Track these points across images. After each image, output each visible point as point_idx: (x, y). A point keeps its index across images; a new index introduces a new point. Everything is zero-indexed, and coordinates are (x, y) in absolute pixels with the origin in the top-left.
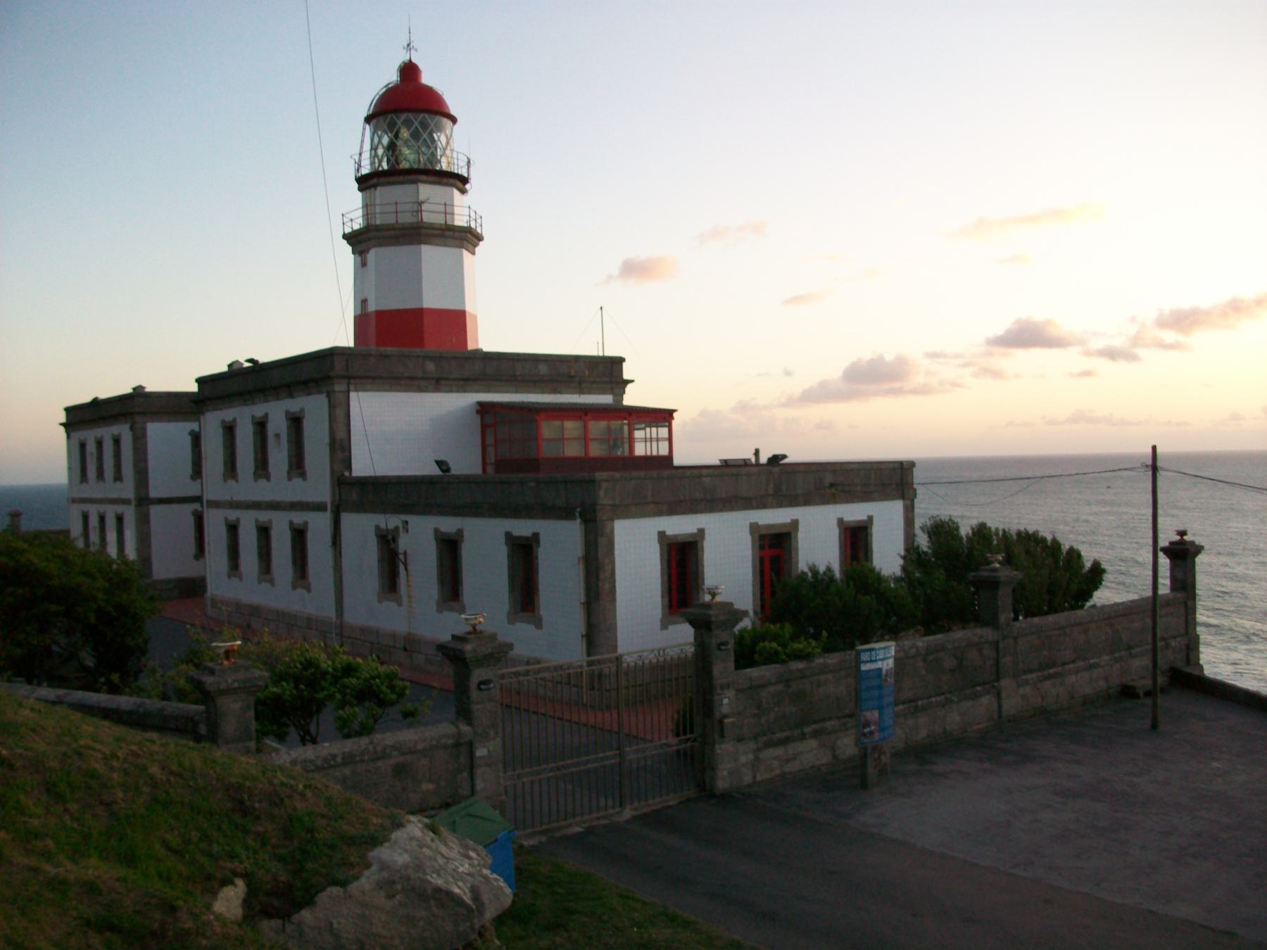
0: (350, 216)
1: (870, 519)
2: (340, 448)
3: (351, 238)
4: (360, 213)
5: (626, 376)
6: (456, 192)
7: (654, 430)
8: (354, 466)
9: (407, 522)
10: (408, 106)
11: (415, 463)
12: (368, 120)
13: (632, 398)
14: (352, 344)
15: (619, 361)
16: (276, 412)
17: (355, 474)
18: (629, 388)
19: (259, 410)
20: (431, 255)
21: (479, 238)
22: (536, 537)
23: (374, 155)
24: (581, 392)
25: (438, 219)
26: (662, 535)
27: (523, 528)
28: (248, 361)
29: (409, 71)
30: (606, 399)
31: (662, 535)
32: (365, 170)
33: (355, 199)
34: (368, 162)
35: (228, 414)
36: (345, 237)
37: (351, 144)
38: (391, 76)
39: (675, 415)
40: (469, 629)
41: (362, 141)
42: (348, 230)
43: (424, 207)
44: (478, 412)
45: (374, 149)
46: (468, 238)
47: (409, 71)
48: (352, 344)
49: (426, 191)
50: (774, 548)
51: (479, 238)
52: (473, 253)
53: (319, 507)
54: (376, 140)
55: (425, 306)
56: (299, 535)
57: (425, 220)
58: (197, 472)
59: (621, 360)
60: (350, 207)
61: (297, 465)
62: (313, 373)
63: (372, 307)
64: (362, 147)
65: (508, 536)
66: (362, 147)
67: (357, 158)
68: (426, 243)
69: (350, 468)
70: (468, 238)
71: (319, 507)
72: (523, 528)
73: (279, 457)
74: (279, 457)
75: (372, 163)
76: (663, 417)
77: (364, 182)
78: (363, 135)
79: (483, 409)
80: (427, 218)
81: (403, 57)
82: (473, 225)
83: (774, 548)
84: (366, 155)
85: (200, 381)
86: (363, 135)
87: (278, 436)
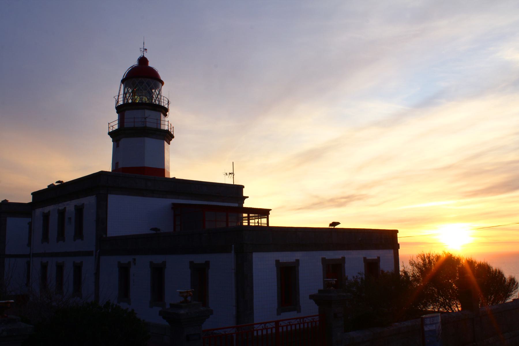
0: (112, 124)
1: (379, 258)
2: (101, 222)
3: (111, 134)
4: (117, 122)
5: (245, 194)
6: (162, 115)
7: (260, 220)
8: (108, 233)
9: (135, 260)
10: (142, 78)
11: (142, 228)
12: (123, 81)
13: (247, 204)
14: (110, 171)
15: (242, 187)
16: (70, 206)
17: (108, 235)
18: (246, 201)
19: (61, 206)
20: (150, 142)
21: (172, 137)
22: (207, 263)
23: (124, 98)
24: (223, 202)
25: (154, 126)
26: (277, 262)
27: (200, 259)
28: (57, 182)
29: (143, 61)
30: (236, 205)
31: (277, 262)
32: (121, 103)
33: (115, 116)
34: (122, 99)
35: (46, 209)
36: (110, 134)
37: (113, 93)
38: (135, 62)
39: (270, 212)
40: (182, 299)
41: (120, 90)
42: (111, 131)
43: (147, 120)
44: (172, 208)
45: (125, 94)
46: (168, 136)
47: (143, 61)
48: (110, 171)
49: (148, 113)
50: (334, 269)
51: (172, 137)
52: (169, 144)
53: (89, 254)
54: (126, 90)
55: (146, 166)
56: (78, 269)
57: (147, 126)
58: (29, 244)
59: (243, 187)
60: (113, 120)
61: (79, 234)
62: (92, 185)
63: (120, 166)
64: (119, 93)
65: (191, 263)
66: (119, 93)
67: (117, 97)
68: (147, 137)
69: (106, 233)
70: (168, 136)
71: (89, 254)
72: (200, 259)
73: (70, 229)
74: (70, 229)
75: (124, 101)
76: (264, 213)
77: (119, 109)
78: (120, 88)
79: (175, 206)
80: (149, 125)
81: (139, 55)
82: (170, 130)
83: (334, 269)
84: (121, 96)
85: (34, 194)
86: (120, 88)
87: (70, 219)
